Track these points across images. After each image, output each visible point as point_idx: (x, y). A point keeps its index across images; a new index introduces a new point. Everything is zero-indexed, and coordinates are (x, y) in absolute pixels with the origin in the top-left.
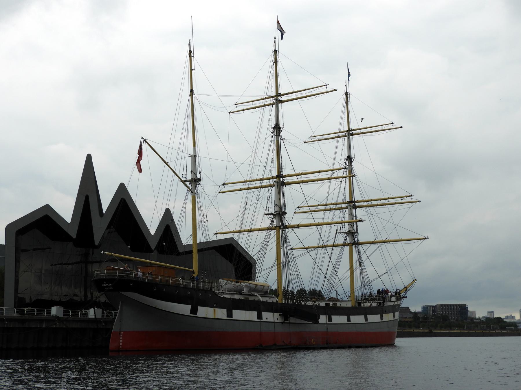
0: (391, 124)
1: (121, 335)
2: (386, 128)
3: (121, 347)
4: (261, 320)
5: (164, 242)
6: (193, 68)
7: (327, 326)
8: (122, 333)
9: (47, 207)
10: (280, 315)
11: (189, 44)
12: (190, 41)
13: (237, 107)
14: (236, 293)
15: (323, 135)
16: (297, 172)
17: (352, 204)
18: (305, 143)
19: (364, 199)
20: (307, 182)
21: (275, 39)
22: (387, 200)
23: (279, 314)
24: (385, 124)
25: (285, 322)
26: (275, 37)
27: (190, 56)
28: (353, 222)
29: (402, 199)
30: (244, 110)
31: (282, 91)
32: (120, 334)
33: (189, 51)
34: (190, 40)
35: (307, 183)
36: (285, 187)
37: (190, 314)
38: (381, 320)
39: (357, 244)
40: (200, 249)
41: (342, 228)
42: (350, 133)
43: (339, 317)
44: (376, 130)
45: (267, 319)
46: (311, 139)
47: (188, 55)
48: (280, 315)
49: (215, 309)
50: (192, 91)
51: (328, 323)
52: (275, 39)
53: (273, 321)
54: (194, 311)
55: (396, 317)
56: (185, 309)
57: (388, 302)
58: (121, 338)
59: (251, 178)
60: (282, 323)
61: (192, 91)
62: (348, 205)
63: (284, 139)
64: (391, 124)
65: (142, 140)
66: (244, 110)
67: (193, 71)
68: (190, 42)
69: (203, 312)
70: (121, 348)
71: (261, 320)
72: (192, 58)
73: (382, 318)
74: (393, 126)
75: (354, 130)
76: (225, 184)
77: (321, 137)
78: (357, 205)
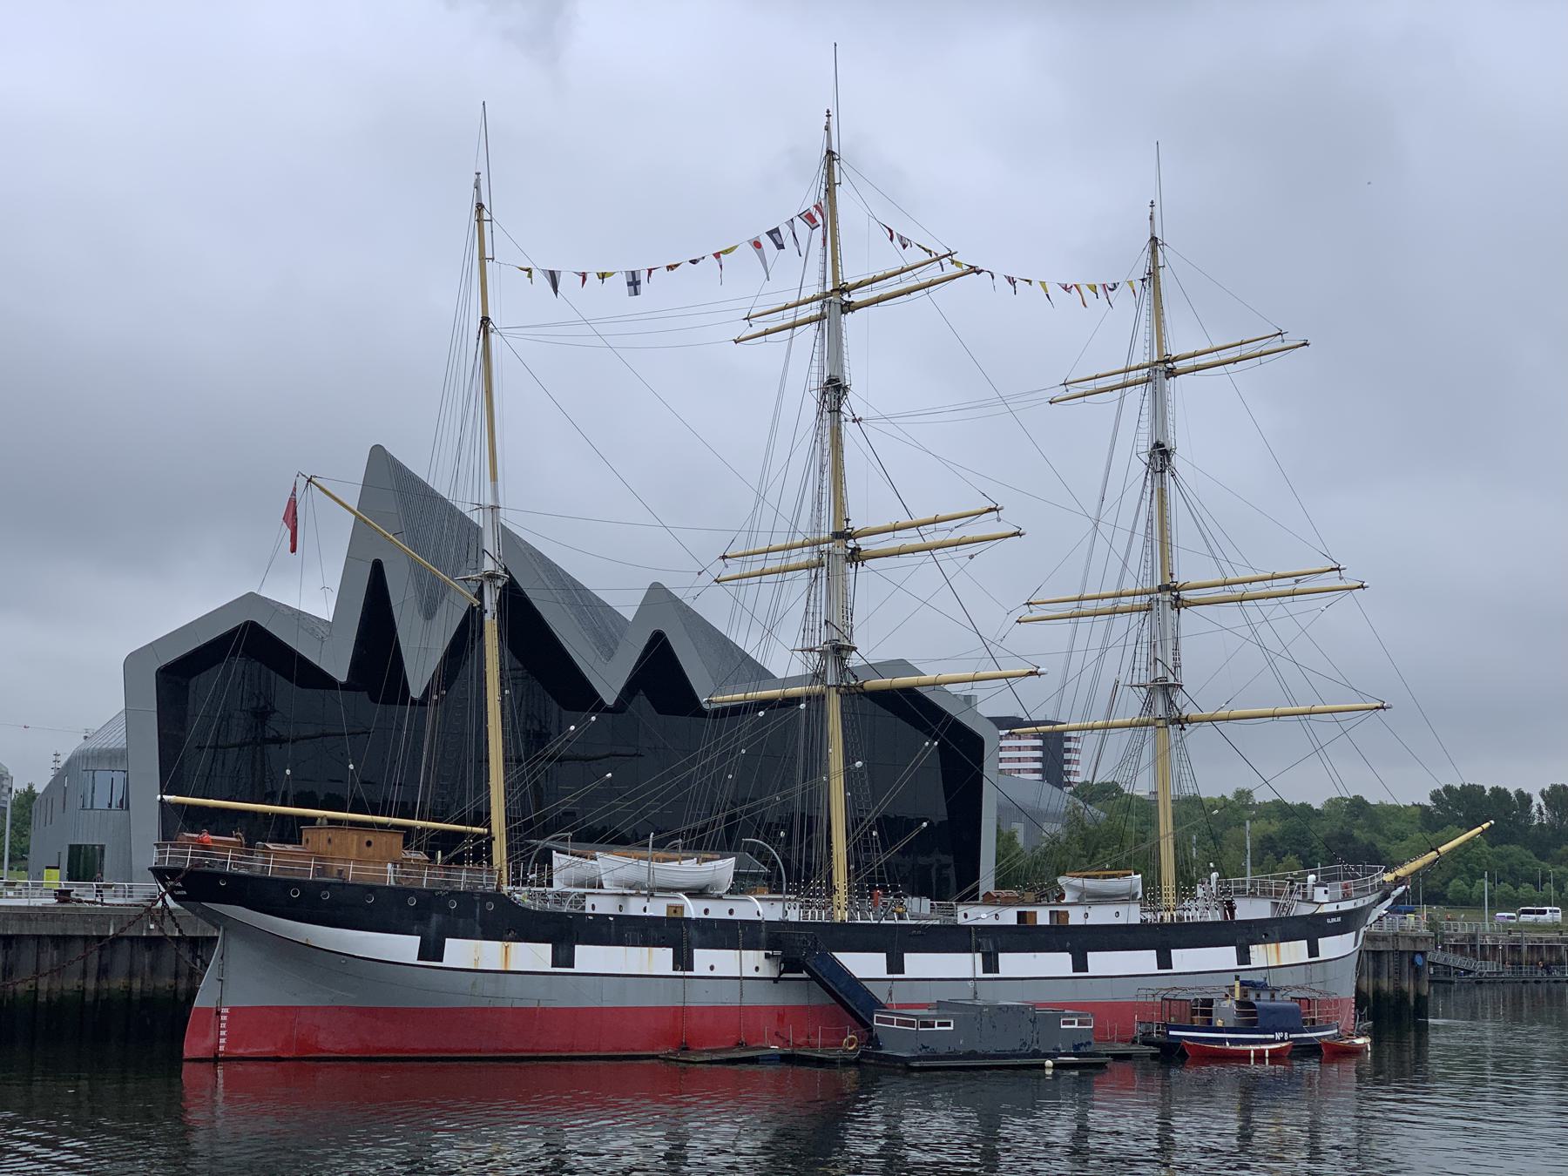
0: (1276, 335)
1: (224, 1018)
2: (1265, 349)
3: (221, 1048)
4: (688, 973)
5: (288, 766)
6: (488, 255)
7: (975, 985)
9: (133, 662)
10: (766, 957)
11: (477, 187)
12: (478, 177)
13: (751, 325)
14: (634, 892)
15: (1096, 377)
16: (919, 518)
17: (1173, 595)
18: (1051, 403)
19: (1236, 578)
20: (913, 552)
21: (828, 116)
22: (1269, 583)
23: (762, 953)
24: (331, 491)
25: (784, 976)
26: (828, 111)
27: (480, 220)
28: (1164, 649)
29: (1297, 581)
30: (766, 333)
31: (850, 276)
32: (219, 1013)
33: (474, 208)
34: (478, 174)
35: (912, 554)
36: (863, 565)
37: (419, 958)
38: (1311, 956)
39: (1181, 722)
40: (950, 716)
41: (1136, 671)
42: (1166, 367)
43: (1035, 956)
44: (1236, 355)
45: (712, 968)
46: (1067, 391)
47: (474, 218)
48: (767, 956)
49: (506, 944)
50: (485, 321)
51: (979, 974)
52: (828, 116)
53: (739, 975)
54: (431, 950)
55: (1320, 954)
56: (404, 947)
57: (1304, 904)
58: (223, 1025)
59: (752, 545)
60: (775, 980)
61: (485, 321)
62: (1151, 599)
63: (860, 419)
64: (1276, 335)
65: (302, 482)
66: (766, 333)
67: (489, 264)
68: (478, 181)
69: (460, 952)
70: (222, 1052)
71: (688, 973)
72: (487, 225)
73: (1313, 951)
74: (1283, 341)
75: (1176, 359)
76: (726, 557)
77: (1090, 386)
78: (1188, 598)
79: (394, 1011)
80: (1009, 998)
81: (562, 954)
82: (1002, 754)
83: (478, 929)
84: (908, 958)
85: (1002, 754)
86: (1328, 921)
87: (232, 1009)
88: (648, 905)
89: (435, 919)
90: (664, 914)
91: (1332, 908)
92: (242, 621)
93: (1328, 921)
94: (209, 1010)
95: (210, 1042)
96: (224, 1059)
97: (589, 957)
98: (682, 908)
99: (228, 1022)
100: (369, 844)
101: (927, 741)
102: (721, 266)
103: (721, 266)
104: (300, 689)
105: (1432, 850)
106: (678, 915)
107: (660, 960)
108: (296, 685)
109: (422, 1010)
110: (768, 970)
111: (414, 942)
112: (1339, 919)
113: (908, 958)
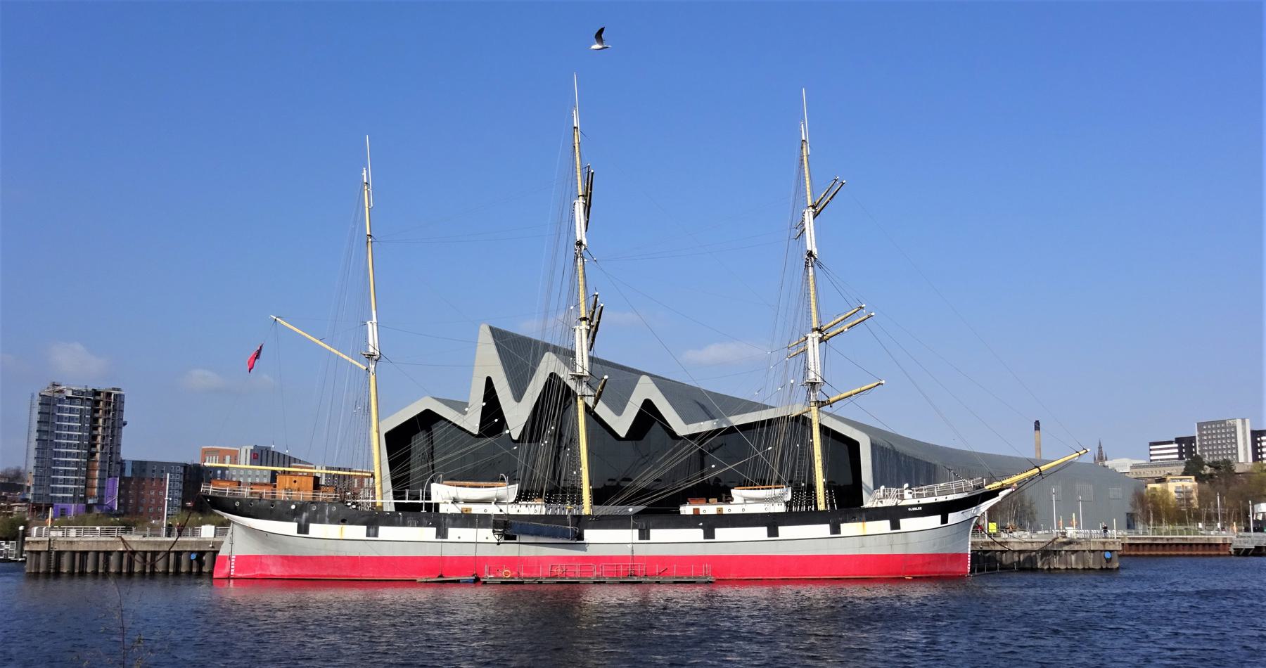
3: (232, 574)
8: (233, 557)
32: (230, 558)
48: (494, 532)
56: (290, 528)
69: (316, 530)
79: (294, 557)
80: (386, 551)
81: (372, 531)
82: (1152, 452)
83: (327, 519)
84: (717, 531)
85: (1152, 452)
86: (910, 509)
87: (237, 556)
88: (520, 509)
89: (305, 515)
90: (692, 513)
91: (915, 502)
92: (1034, 424)
93: (910, 509)
94: (225, 557)
95: (227, 570)
96: (232, 578)
97: (721, 533)
98: (470, 510)
99: (235, 563)
100: (295, 482)
101: (514, 450)
102: (258, 355)
103: (258, 355)
104: (615, 440)
105: (1036, 467)
106: (468, 512)
107: (761, 532)
108: (411, 442)
109: (311, 558)
110: (493, 539)
111: (295, 525)
112: (920, 508)
113: (717, 531)
